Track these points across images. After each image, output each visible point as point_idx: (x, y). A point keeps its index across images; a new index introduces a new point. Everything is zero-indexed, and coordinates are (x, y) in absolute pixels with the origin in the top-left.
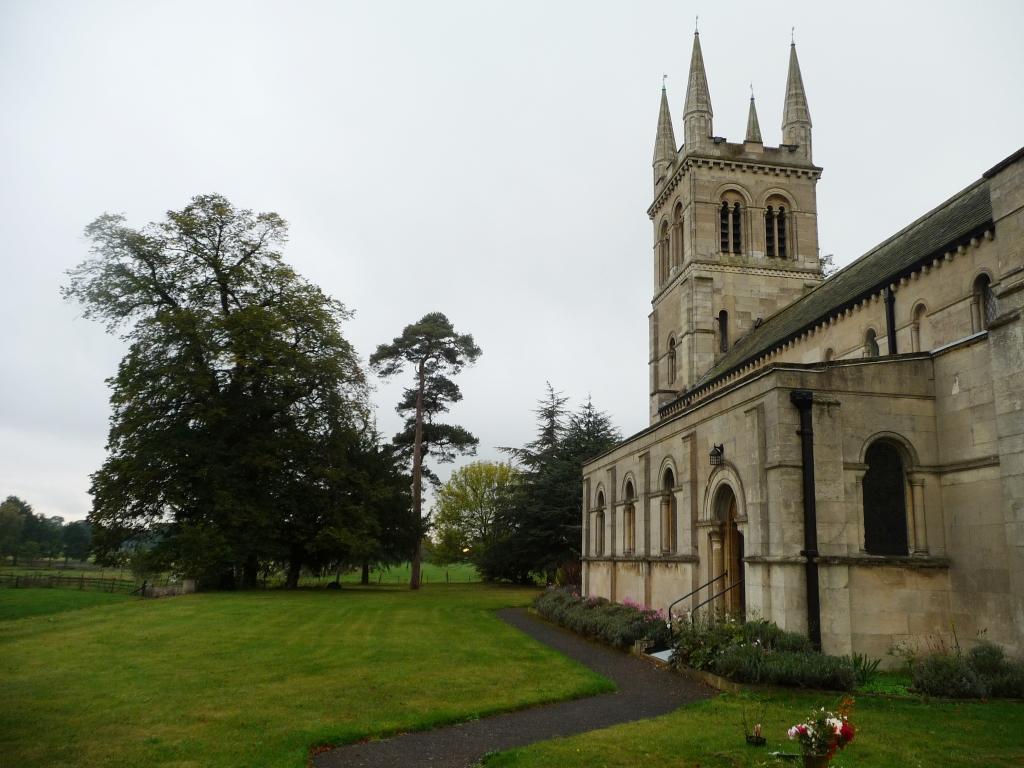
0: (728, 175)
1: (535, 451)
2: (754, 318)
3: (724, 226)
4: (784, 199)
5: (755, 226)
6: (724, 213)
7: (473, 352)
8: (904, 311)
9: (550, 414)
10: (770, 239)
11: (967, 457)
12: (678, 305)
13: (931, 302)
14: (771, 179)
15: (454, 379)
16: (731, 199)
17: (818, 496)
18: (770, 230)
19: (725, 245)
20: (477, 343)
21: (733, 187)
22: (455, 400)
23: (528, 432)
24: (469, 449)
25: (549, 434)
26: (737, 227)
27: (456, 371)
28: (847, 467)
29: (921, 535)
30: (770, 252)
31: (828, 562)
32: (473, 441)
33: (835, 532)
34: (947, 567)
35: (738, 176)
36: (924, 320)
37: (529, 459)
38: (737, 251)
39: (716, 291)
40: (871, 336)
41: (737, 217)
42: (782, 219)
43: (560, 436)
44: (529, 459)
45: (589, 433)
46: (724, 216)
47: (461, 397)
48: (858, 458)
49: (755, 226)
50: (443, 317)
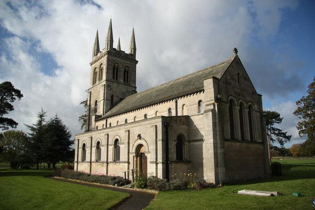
0: (116, 59)
1: (35, 127)
2: (120, 97)
3: (114, 72)
4: (129, 67)
5: (121, 74)
6: (125, 71)
7: (20, 95)
8: (180, 105)
9: (41, 116)
10: (125, 77)
11: (196, 139)
12: (99, 91)
13: (187, 104)
14: (126, 62)
15: (12, 104)
16: (116, 65)
17: (169, 147)
18: (125, 74)
19: (114, 77)
20: (22, 93)
21: (117, 62)
22: (11, 110)
23: (34, 121)
24: (14, 126)
25: (40, 123)
26: (117, 72)
27: (13, 101)
28: (175, 140)
29: (185, 156)
30: (124, 81)
31: (171, 162)
32: (16, 124)
33: (172, 156)
34: (190, 162)
35: (119, 59)
36: (184, 107)
37: (33, 129)
38: (117, 79)
39: (111, 89)
40: (170, 110)
41: (117, 70)
42: (128, 72)
43: (44, 123)
44: (33, 129)
45: (56, 123)
46: (114, 69)
47: (13, 109)
48: (176, 139)
49: (121, 74)
50: (11, 83)
